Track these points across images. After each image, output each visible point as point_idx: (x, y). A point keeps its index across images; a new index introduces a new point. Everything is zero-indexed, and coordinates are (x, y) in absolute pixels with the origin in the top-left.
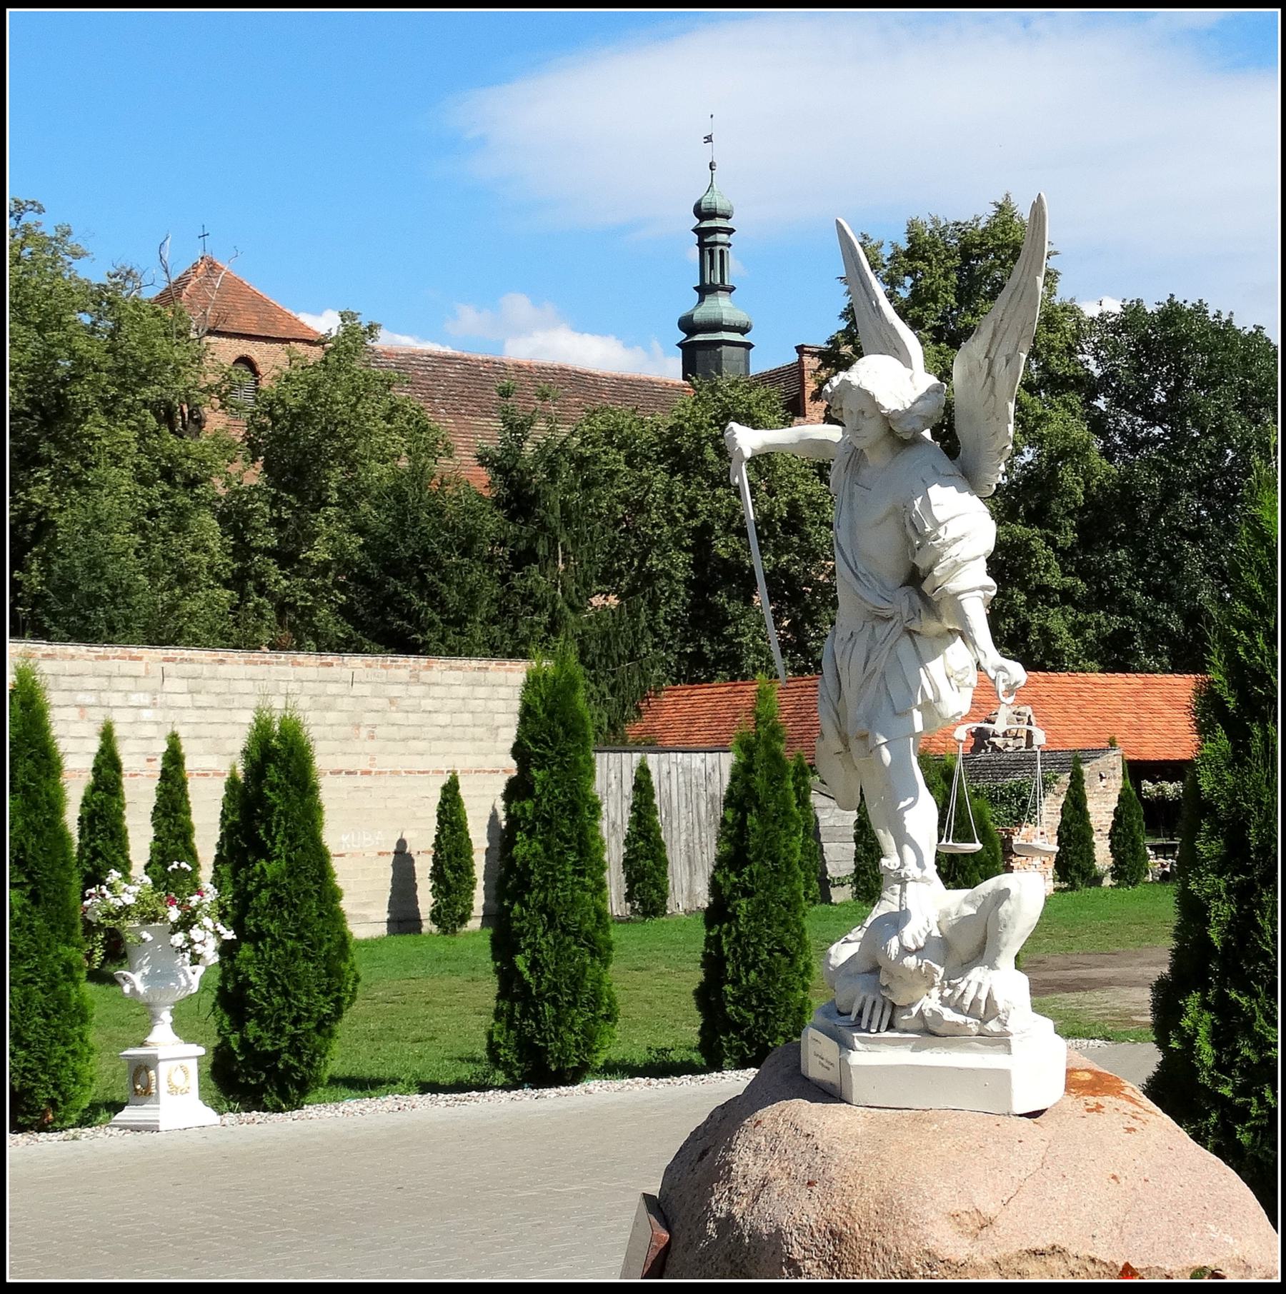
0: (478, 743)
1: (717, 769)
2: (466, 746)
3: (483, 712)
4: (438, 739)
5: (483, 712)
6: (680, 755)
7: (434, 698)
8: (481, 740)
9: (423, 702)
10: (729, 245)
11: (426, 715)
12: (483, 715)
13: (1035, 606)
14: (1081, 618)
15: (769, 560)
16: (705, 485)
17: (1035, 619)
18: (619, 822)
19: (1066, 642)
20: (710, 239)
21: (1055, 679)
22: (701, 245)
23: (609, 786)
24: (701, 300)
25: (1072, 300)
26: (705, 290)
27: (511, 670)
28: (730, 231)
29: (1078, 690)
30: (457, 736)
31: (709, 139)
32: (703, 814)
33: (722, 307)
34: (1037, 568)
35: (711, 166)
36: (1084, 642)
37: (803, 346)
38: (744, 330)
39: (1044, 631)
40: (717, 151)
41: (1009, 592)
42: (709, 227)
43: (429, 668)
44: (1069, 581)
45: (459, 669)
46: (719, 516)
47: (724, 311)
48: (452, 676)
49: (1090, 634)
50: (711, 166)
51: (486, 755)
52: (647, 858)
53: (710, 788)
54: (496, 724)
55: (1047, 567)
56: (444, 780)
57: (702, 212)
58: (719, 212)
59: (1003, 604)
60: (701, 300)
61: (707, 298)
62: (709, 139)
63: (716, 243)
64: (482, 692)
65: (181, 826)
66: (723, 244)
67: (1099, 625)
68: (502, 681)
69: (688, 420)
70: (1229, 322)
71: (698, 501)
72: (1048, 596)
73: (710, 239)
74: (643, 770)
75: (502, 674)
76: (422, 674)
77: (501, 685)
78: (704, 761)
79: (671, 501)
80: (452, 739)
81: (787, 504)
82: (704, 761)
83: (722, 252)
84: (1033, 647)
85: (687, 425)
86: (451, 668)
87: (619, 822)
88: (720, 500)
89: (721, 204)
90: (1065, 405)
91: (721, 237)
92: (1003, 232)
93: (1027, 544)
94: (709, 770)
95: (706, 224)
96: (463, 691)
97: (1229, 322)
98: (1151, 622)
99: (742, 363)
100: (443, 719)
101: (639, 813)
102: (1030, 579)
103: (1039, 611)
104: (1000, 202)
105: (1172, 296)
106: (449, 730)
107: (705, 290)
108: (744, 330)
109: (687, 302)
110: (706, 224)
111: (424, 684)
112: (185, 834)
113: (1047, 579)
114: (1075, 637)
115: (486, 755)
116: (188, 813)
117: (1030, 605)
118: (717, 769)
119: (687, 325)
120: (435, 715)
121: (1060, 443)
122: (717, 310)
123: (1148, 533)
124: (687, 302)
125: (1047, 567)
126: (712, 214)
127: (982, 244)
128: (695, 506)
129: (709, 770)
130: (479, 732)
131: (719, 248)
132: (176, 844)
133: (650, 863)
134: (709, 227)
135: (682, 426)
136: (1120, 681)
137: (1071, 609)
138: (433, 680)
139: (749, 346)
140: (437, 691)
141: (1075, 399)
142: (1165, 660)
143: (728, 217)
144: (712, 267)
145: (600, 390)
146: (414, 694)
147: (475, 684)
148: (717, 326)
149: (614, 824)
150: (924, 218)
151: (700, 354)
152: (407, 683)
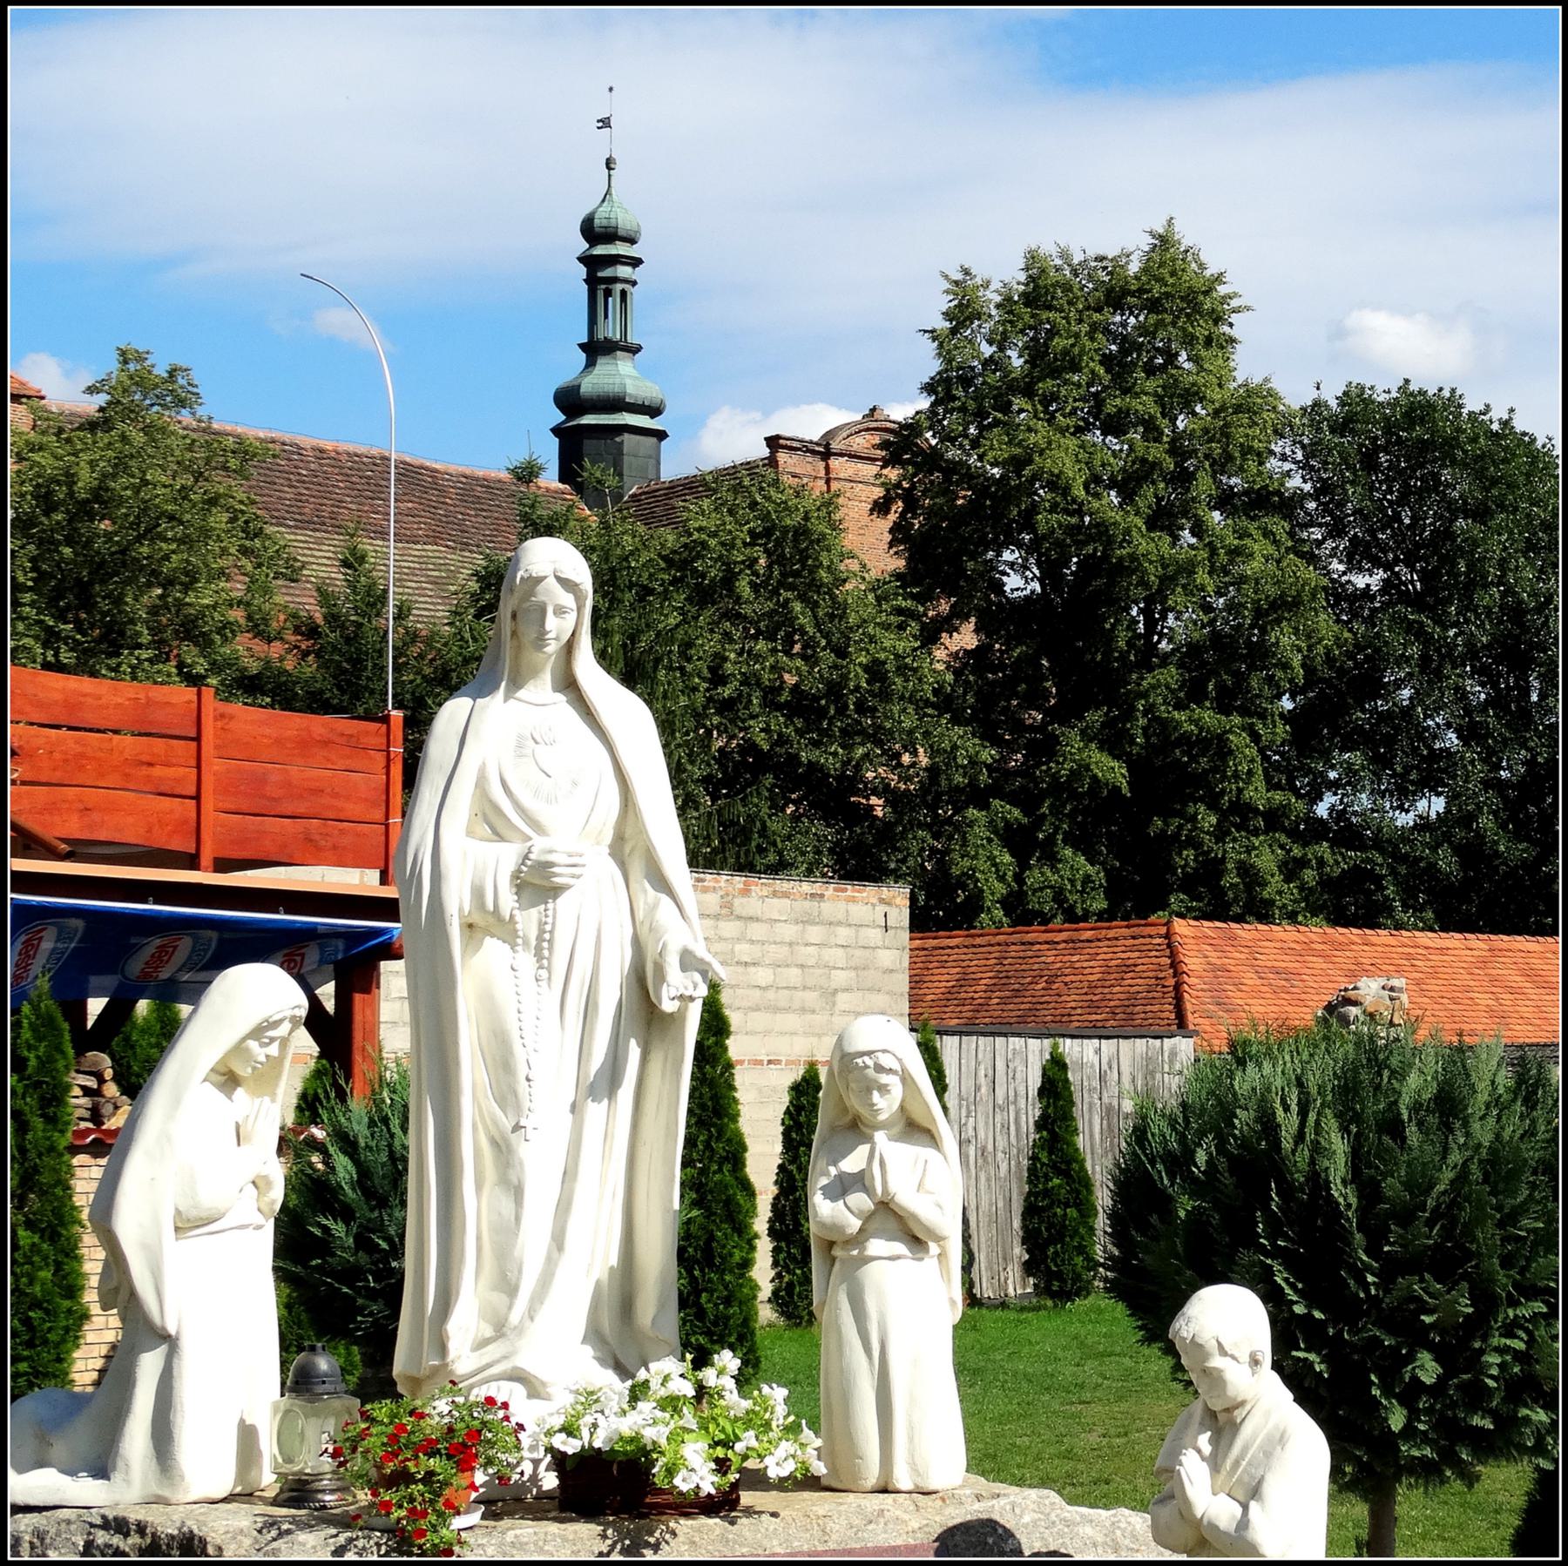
0: (809, 1017)
1: (1115, 1066)
2: (791, 1021)
3: (817, 966)
4: (757, 1009)
5: (817, 966)
6: (1068, 1041)
7: (752, 942)
8: (813, 1012)
9: (738, 947)
10: (634, 283)
11: (740, 969)
12: (818, 971)
13: (1229, 833)
14: (1297, 852)
15: (835, 754)
16: (737, 635)
17: (1232, 851)
18: (990, 1147)
19: (1275, 886)
20: (607, 273)
21: (1374, 939)
22: (592, 281)
23: (977, 1088)
24: (590, 364)
25: (1267, 380)
26: (596, 349)
27: (853, 900)
28: (636, 262)
29: (1409, 957)
30: (783, 1004)
31: (605, 123)
32: (1097, 1136)
33: (619, 375)
34: (1236, 775)
35: (609, 164)
36: (1301, 889)
37: (778, 437)
38: (654, 411)
39: (1245, 869)
40: (618, 141)
41: (1191, 810)
42: (605, 255)
43: (746, 892)
44: (1278, 796)
45: (786, 895)
46: (758, 684)
47: (628, 382)
48: (777, 907)
49: (1309, 875)
50: (609, 164)
51: (819, 1036)
52: (1067, 1205)
53: (1105, 1095)
54: (834, 985)
55: (1250, 773)
56: (797, 1074)
57: (591, 231)
58: (621, 232)
59: (1180, 827)
60: (590, 364)
61: (601, 361)
62: (605, 123)
63: (615, 280)
64: (815, 933)
65: (729, 1141)
66: (626, 281)
67: (1321, 862)
68: (841, 916)
69: (714, 535)
70: (1506, 424)
71: (726, 659)
72: (1245, 819)
73: (607, 273)
74: (1056, 1070)
75: (842, 905)
76: (737, 902)
77: (839, 923)
78: (1098, 1051)
79: (689, 660)
80: (776, 1010)
81: (866, 669)
82: (1098, 1051)
83: (624, 293)
84: (1231, 894)
85: (713, 542)
86: (775, 894)
87: (990, 1147)
88: (758, 658)
89: (624, 219)
90: (1267, 533)
91: (623, 271)
92: (1173, 274)
93: (1221, 739)
94: (1105, 1067)
95: (600, 250)
96: (789, 932)
97: (1506, 424)
98: (1404, 858)
99: (653, 461)
100: (763, 975)
101: (1052, 1132)
102: (1223, 791)
103: (1234, 840)
104: (1161, 231)
105: (1407, 381)
106: (771, 994)
107: (596, 349)
108: (654, 411)
109: (568, 365)
110: (600, 250)
111: (739, 918)
112: (735, 1155)
113: (1249, 793)
114: (1287, 880)
115: (819, 1036)
116: (735, 1117)
117: (1220, 834)
118: (1115, 1066)
119: (569, 400)
120: (752, 969)
121: (1273, 591)
122: (617, 381)
123: (1397, 729)
124: (568, 365)
125: (1250, 773)
126: (610, 236)
127: (1141, 291)
128: (720, 667)
129: (1105, 1067)
130: (811, 997)
131: (619, 287)
132: (720, 1170)
133: (1072, 1212)
134: (605, 255)
135: (704, 544)
136: (1457, 944)
137: (1283, 838)
138: (751, 913)
139: (661, 435)
140: (757, 931)
141: (1280, 527)
142: (1430, 915)
143: (632, 241)
144: (606, 317)
145: (442, 491)
146: (726, 934)
147: (806, 921)
148: (616, 404)
149: (984, 1150)
150: (1048, 248)
151: (589, 445)
152: (717, 917)
